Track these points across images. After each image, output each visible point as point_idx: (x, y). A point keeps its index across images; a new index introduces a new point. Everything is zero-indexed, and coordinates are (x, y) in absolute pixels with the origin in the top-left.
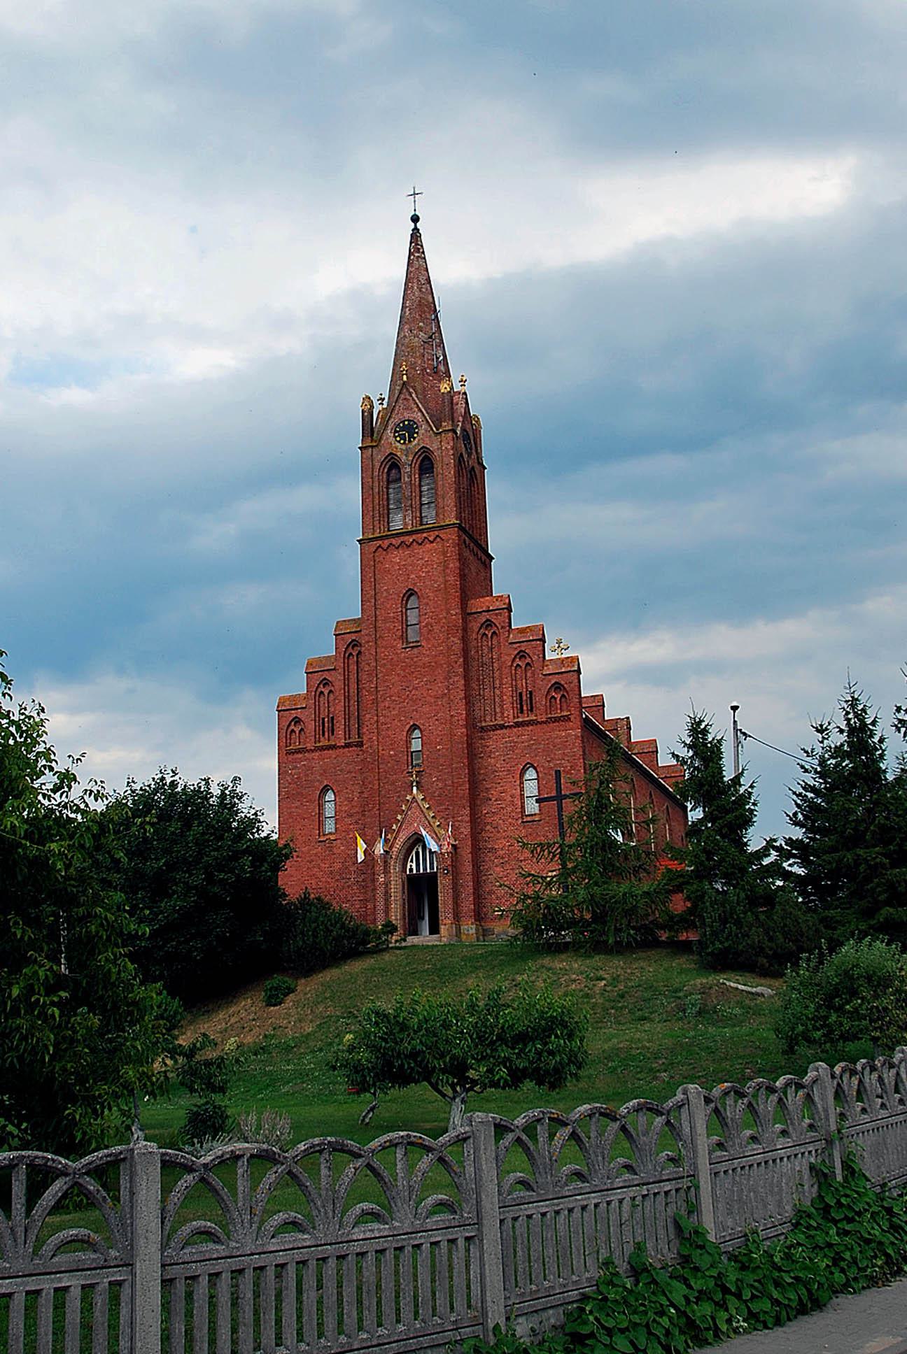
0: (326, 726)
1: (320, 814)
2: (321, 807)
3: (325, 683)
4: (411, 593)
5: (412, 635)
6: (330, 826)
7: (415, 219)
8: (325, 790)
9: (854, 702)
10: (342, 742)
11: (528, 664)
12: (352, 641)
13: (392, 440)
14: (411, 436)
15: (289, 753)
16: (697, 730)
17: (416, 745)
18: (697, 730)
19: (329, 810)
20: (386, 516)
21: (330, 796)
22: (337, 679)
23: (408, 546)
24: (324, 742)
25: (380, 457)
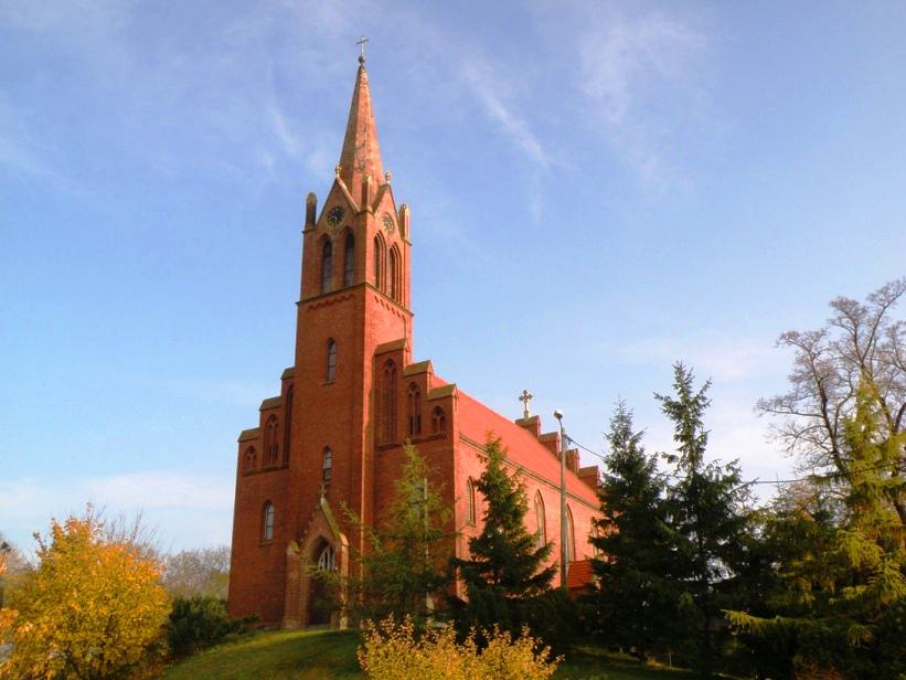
0: (271, 452)
1: (262, 524)
2: (263, 517)
3: (273, 418)
4: (331, 342)
5: (331, 376)
6: (270, 534)
7: (361, 60)
8: (268, 503)
9: (621, 418)
10: (280, 466)
11: (418, 393)
12: (288, 378)
14: (339, 220)
15: (244, 476)
16: (834, 304)
17: (328, 464)
18: (834, 304)
19: (270, 520)
20: (322, 280)
21: (271, 509)
22: (281, 414)
23: (332, 304)
24: (251, 469)
25: (317, 237)
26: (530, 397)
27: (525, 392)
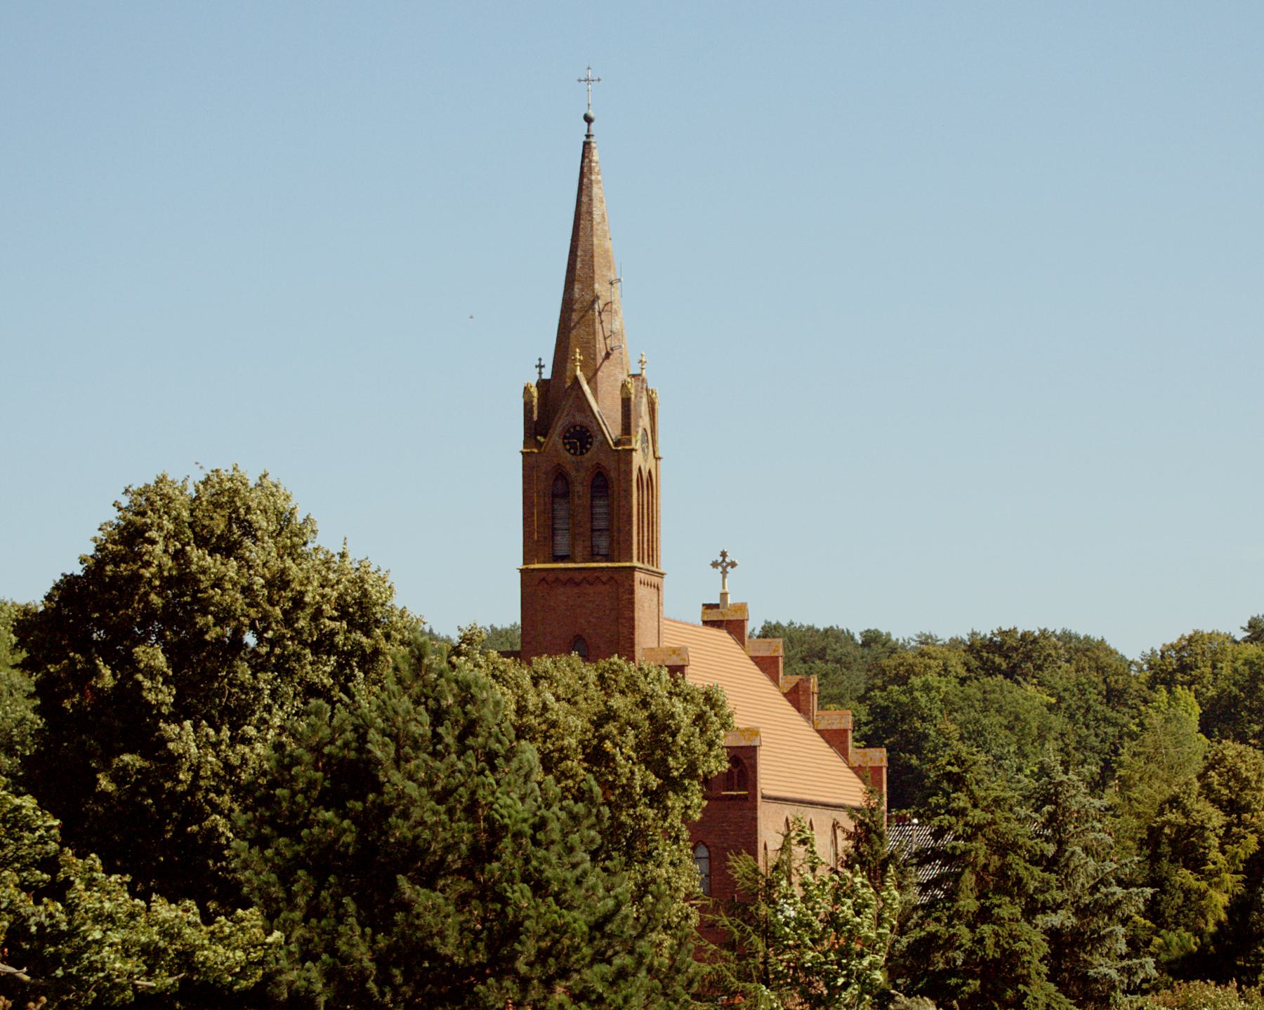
13: (560, 446)
23: (577, 584)
26: (733, 565)
27: (724, 554)
